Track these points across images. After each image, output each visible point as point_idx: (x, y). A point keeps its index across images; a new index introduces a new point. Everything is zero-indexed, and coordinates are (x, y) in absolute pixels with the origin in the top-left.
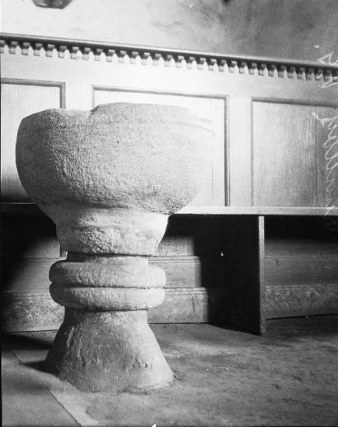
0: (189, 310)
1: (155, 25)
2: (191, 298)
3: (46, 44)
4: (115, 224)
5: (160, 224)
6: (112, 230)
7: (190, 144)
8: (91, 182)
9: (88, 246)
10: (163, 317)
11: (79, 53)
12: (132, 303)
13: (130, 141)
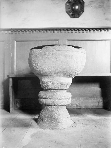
0: (97, 104)
1: (106, 19)
2: (97, 100)
3: (75, 29)
4: (50, 81)
5: (70, 80)
6: (50, 82)
7: (70, 57)
8: (41, 69)
9: (45, 87)
10: (88, 106)
11: (63, 31)
12: (56, 104)
13: (50, 57)
